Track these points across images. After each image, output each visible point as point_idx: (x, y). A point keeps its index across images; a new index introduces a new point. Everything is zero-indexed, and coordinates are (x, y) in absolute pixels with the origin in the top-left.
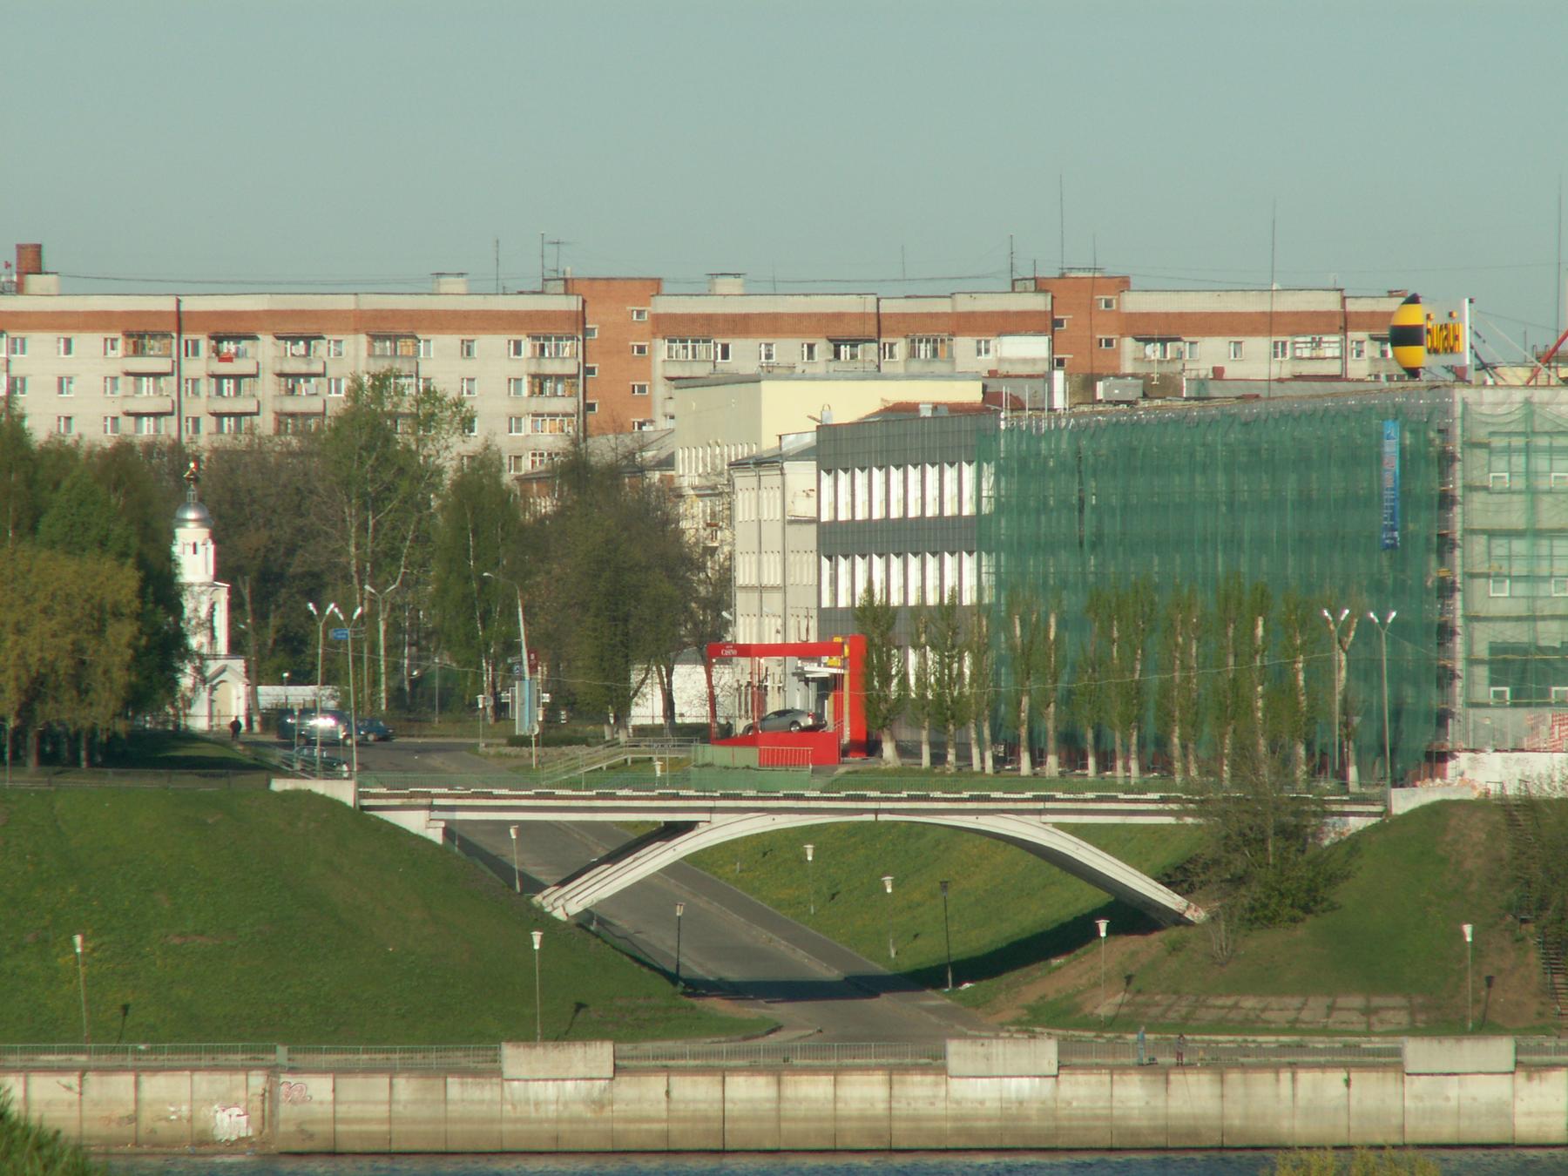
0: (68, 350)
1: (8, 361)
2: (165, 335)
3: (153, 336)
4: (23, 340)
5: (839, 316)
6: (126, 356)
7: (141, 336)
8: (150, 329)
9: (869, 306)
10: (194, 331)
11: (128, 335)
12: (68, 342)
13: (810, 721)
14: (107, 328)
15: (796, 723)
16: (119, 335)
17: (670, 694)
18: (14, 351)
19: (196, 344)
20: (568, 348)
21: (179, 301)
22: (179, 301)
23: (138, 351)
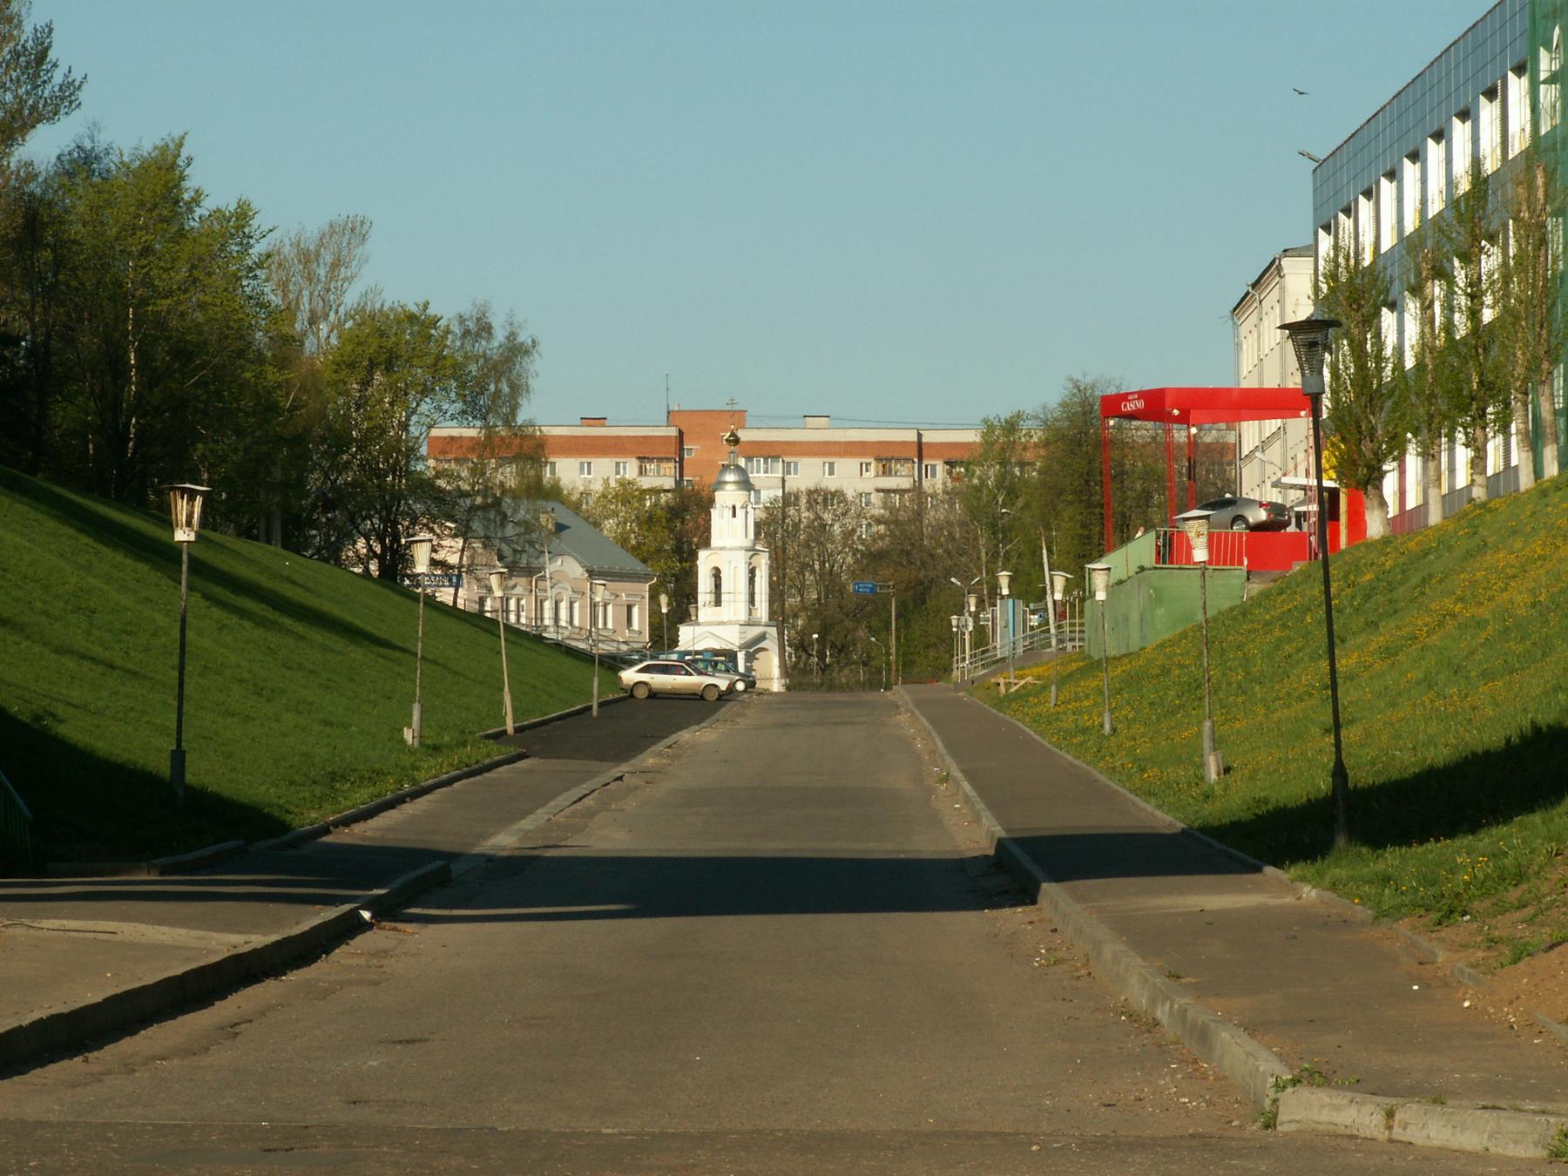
0: (831, 472)
1: (784, 481)
2: (907, 460)
3: (898, 460)
4: (796, 464)
5: (646, 439)
6: (877, 475)
7: (889, 460)
8: (896, 455)
9: (911, 436)
10: (932, 458)
11: (878, 459)
12: (832, 465)
13: (1262, 515)
14: (862, 455)
15: (1239, 518)
16: (871, 460)
17: (1535, 472)
18: (789, 473)
19: (934, 467)
20: (903, 469)
21: (920, 436)
22: (920, 436)
23: (886, 472)
